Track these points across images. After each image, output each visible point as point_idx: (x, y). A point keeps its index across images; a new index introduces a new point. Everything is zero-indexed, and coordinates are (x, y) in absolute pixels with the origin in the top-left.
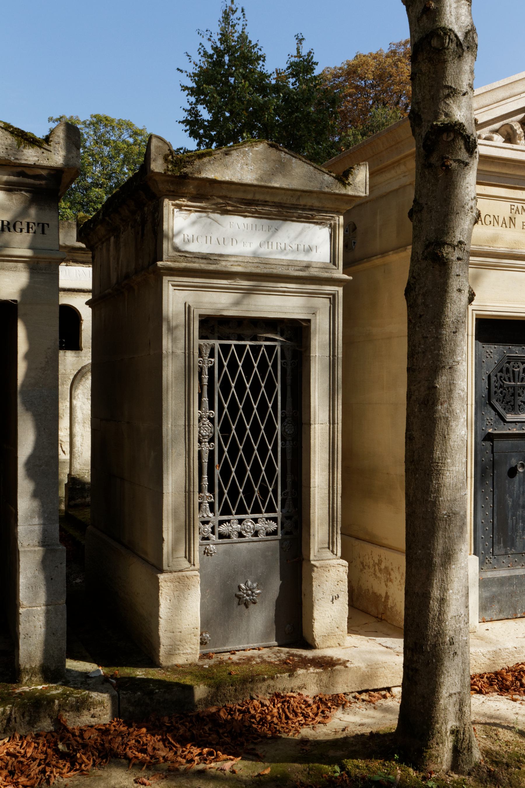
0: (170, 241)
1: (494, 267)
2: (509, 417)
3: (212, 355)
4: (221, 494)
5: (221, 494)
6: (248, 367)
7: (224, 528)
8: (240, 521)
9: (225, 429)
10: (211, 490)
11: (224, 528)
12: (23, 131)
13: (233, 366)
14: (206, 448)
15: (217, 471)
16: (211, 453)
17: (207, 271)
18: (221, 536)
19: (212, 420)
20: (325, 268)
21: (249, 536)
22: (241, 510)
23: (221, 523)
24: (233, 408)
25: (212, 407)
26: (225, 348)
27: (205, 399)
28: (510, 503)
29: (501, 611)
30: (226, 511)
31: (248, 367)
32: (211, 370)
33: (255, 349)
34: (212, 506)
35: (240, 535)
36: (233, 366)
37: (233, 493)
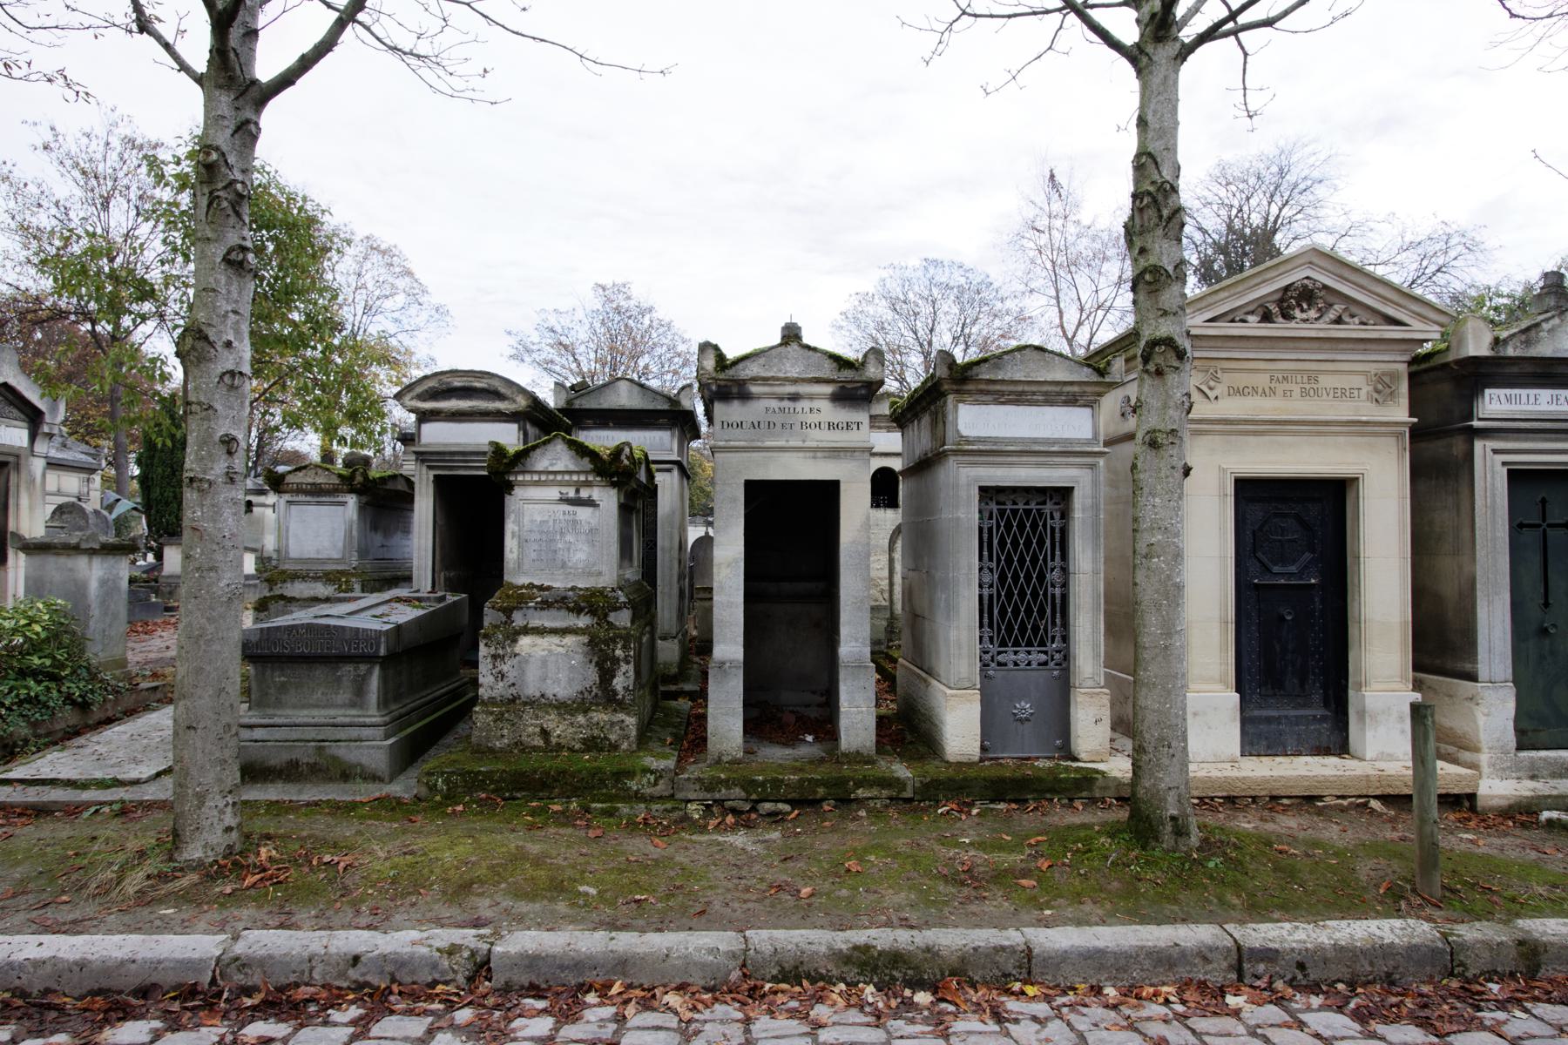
0: (628, 764)
1: (1206, 433)
2: (1276, 569)
3: (991, 518)
4: (999, 629)
5: (999, 629)
6: (1021, 526)
7: (1000, 658)
8: (1016, 653)
9: (1002, 578)
10: (991, 626)
11: (1000, 658)
12: (1179, 588)
13: (1008, 526)
14: (986, 592)
15: (996, 612)
16: (991, 596)
17: (993, 451)
18: (999, 664)
19: (991, 570)
20: (1088, 442)
21: (1022, 666)
22: (1017, 644)
23: (999, 653)
24: (1009, 561)
25: (991, 559)
26: (1002, 513)
27: (985, 553)
28: (1278, 648)
29: (1268, 747)
30: (1003, 644)
31: (1021, 526)
32: (990, 529)
33: (1028, 512)
34: (991, 639)
35: (1016, 664)
36: (1008, 526)
37: (1010, 629)
